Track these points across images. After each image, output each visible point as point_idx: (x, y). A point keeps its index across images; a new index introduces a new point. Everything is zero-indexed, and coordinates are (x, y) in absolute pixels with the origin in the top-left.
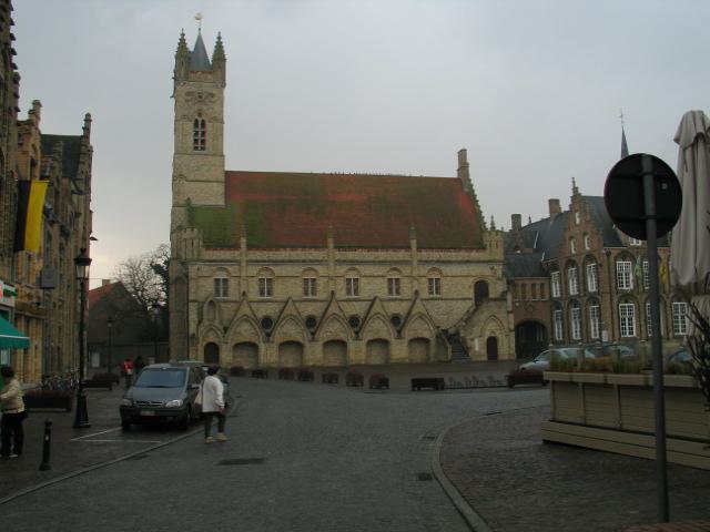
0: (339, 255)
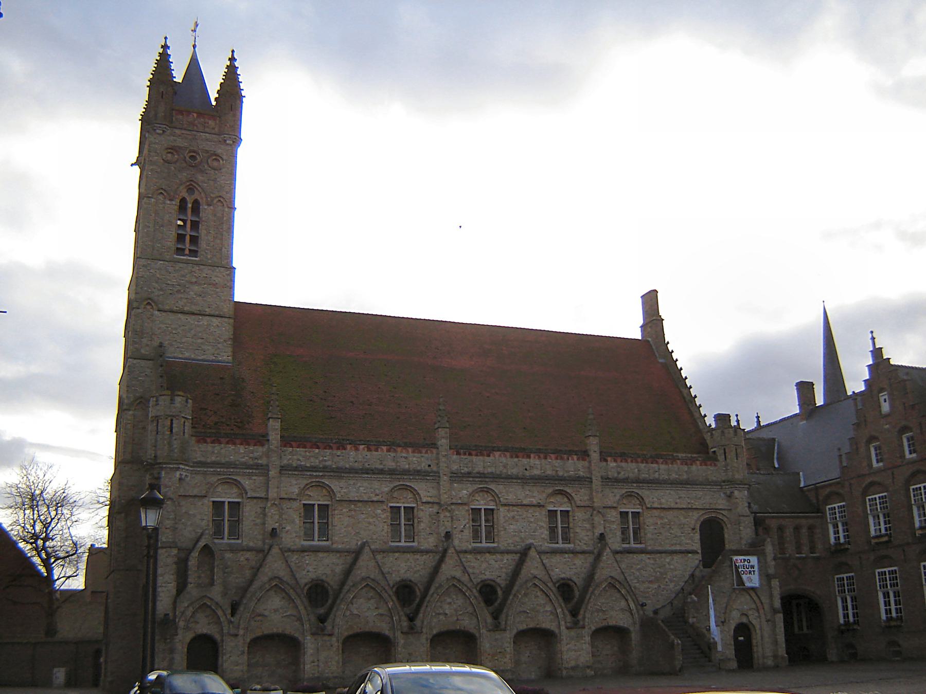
0: (457, 463)
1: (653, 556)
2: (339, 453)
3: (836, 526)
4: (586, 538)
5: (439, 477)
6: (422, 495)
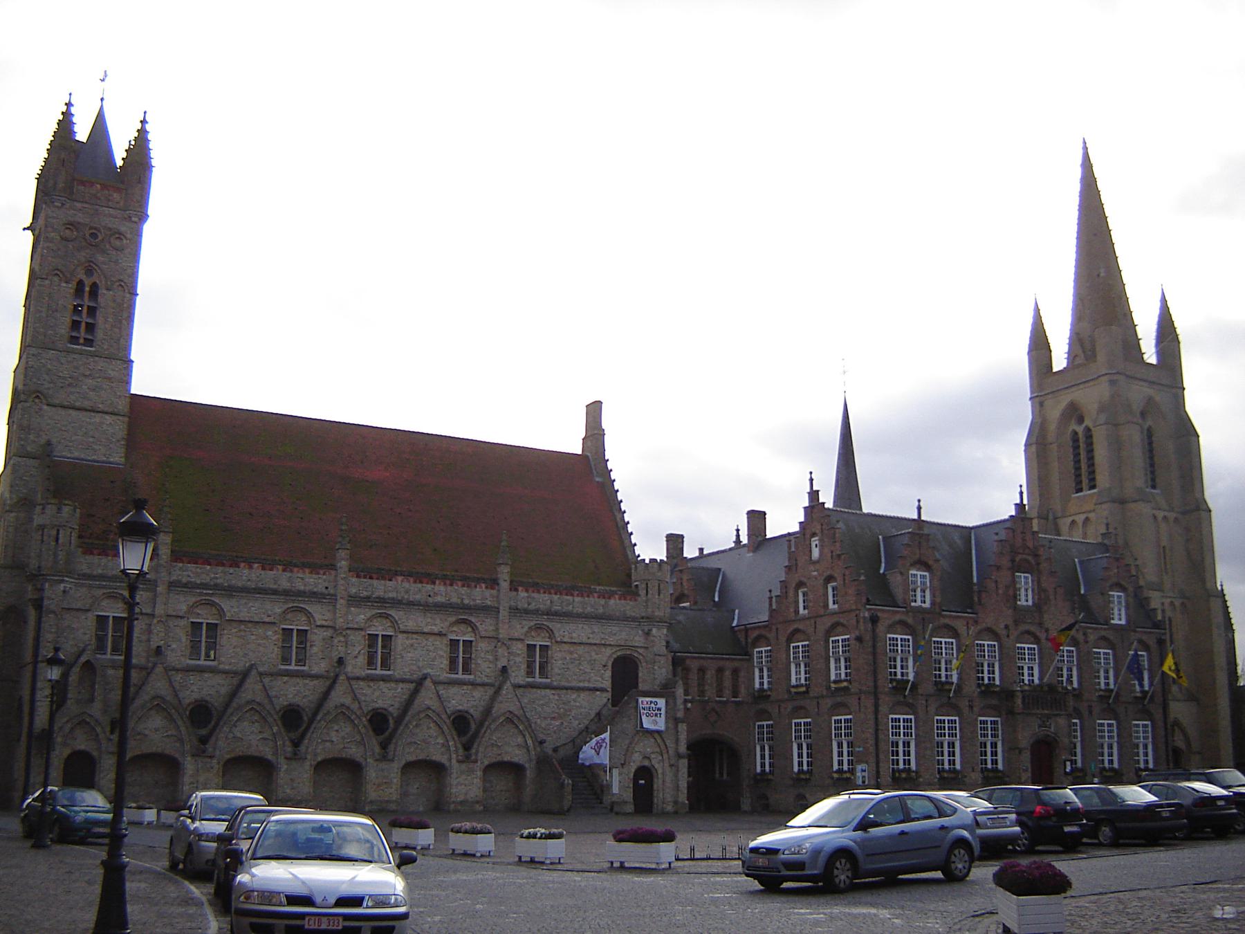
0: (357, 586)
1: (558, 691)
2: (231, 570)
3: (761, 670)
4: (488, 670)
5: (336, 600)
6: (317, 619)
